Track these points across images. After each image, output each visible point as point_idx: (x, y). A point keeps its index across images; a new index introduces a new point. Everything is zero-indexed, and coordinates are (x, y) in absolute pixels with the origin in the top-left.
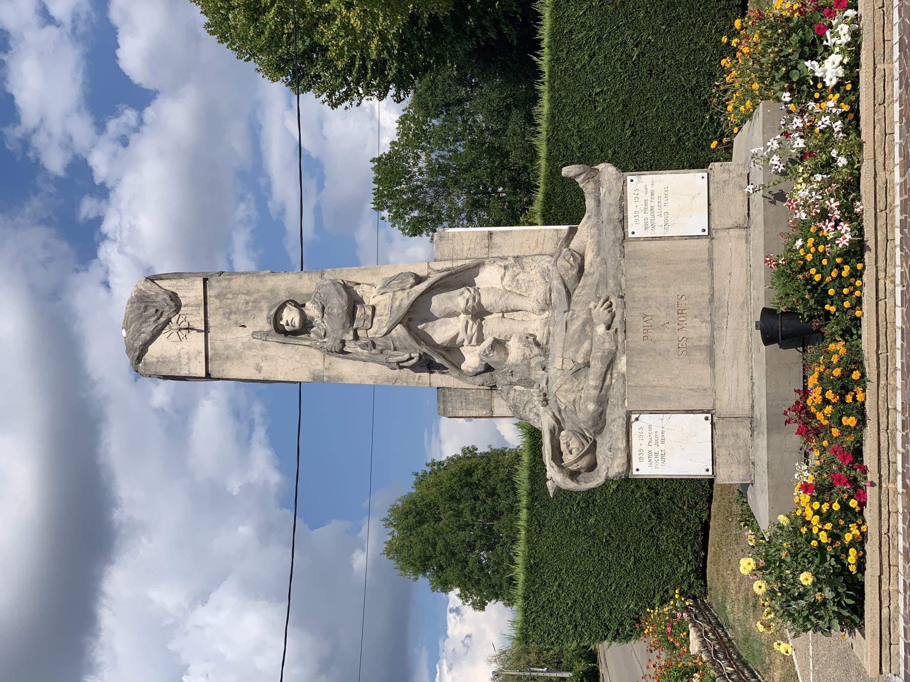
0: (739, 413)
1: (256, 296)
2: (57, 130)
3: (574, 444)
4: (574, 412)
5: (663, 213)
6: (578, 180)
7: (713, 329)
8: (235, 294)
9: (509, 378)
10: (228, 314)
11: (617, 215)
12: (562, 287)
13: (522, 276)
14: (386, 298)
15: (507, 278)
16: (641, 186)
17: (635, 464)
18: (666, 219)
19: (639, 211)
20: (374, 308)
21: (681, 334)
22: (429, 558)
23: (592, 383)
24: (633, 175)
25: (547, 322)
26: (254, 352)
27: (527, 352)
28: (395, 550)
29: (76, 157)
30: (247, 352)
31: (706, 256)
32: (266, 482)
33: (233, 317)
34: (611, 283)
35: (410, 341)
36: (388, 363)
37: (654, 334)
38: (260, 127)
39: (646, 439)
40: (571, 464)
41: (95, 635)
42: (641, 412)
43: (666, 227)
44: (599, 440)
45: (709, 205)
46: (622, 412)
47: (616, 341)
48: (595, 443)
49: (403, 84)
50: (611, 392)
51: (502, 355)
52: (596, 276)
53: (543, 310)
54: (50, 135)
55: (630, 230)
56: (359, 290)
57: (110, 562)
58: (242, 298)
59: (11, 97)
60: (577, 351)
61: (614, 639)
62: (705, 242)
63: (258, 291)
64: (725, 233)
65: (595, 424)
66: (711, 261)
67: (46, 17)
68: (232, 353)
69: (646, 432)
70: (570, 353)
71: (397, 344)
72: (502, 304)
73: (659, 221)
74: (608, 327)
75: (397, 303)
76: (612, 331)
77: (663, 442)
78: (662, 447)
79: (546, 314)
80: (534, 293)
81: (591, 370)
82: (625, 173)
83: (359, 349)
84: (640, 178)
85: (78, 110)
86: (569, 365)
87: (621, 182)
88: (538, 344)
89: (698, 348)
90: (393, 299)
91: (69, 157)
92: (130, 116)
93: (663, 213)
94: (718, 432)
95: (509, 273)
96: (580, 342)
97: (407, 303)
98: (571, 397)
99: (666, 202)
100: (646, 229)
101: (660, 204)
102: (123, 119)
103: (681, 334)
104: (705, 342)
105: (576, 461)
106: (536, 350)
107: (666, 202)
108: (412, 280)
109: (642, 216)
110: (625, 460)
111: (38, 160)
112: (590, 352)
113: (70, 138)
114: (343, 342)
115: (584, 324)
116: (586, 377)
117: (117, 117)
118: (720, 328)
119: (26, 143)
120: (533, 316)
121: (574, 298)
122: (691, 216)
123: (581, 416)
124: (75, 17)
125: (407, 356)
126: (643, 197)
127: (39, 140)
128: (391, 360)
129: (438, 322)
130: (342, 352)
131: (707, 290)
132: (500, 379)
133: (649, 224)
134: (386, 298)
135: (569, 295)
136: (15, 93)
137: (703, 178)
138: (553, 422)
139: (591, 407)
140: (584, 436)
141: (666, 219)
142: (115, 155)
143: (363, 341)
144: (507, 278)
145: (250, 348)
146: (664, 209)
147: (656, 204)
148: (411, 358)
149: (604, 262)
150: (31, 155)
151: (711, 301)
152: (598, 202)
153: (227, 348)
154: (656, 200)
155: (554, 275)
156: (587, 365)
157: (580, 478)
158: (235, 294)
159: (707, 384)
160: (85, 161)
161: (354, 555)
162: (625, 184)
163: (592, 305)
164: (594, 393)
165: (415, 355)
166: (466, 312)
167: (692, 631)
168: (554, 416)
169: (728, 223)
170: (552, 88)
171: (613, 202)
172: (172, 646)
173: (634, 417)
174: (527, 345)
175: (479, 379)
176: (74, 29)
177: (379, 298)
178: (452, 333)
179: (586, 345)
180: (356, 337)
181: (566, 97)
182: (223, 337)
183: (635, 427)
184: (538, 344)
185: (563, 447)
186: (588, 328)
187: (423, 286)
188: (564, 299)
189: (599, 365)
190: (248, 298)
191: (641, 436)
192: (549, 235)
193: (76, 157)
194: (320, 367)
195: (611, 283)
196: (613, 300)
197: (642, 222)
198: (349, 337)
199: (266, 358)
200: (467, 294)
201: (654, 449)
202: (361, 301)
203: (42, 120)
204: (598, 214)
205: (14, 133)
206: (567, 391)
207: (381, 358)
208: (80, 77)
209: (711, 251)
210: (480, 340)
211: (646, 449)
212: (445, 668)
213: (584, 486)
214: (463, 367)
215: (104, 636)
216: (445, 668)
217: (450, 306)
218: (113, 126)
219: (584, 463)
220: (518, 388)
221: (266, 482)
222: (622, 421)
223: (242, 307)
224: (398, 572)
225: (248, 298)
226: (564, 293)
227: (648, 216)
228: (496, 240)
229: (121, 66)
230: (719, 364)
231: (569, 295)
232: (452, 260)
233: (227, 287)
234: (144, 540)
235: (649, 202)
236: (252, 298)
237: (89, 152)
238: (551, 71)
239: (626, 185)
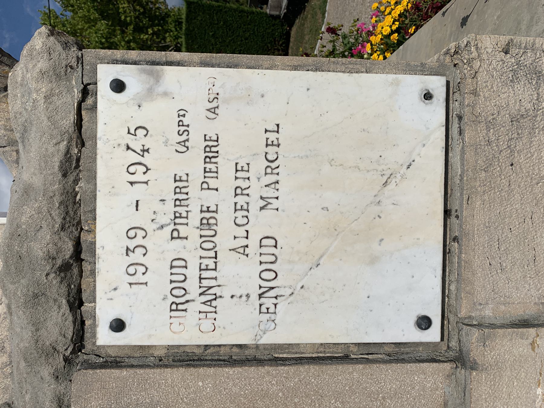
5: (254, 242)
19: (150, 227)
24: (125, 62)
43: (268, 303)
45: (447, 213)
82: (89, 54)
84: (157, 78)
87: (70, 90)
93: (254, 242)
99: (270, 193)
100: (175, 307)
101: (241, 200)
107: (270, 193)
122: (373, 260)
133: (193, 286)
137: (428, 96)
162: (89, 101)
171: (37, 181)
235: (194, 189)
239: (94, 107)
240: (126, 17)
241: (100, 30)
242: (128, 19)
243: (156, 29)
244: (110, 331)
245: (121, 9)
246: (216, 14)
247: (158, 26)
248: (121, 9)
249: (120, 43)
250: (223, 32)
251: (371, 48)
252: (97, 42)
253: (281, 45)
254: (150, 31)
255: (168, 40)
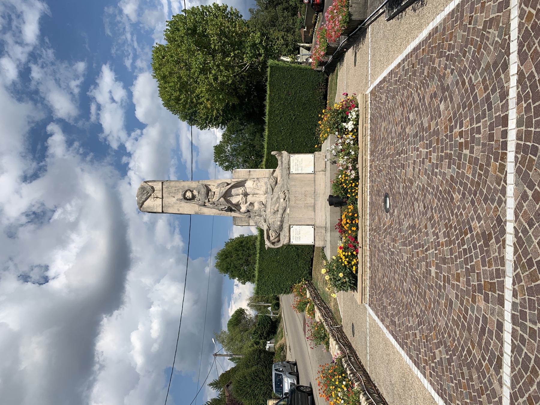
0: (322, 226)
1: (178, 188)
2: (116, 136)
3: (274, 234)
4: (274, 224)
6: (276, 156)
7: (315, 201)
8: (172, 187)
9: (255, 214)
10: (169, 193)
11: (287, 167)
12: (271, 187)
13: (259, 184)
14: (218, 190)
15: (255, 184)
16: (294, 158)
17: (291, 240)
18: (302, 168)
20: (214, 192)
21: (306, 202)
22: (229, 269)
23: (279, 216)
25: (266, 198)
26: (177, 205)
27: (260, 206)
28: (218, 266)
29: (121, 144)
30: (175, 205)
31: (313, 179)
32: (179, 245)
33: (171, 194)
34: (285, 186)
35: (225, 203)
36: (218, 209)
37: (298, 202)
38: (179, 136)
39: (295, 233)
40: (272, 240)
41: (124, 293)
42: (294, 225)
44: (281, 233)
46: (288, 225)
47: (286, 204)
48: (280, 234)
49: (223, 123)
50: (285, 219)
51: (253, 207)
52: (281, 184)
53: (265, 194)
54: (113, 137)
55: (291, 171)
56: (210, 187)
57: (129, 270)
58: (174, 189)
59: (101, 125)
60: (275, 206)
61: (284, 293)
62: (313, 175)
63: (179, 186)
64: (319, 173)
65: (280, 228)
66: (315, 181)
67: (113, 100)
68: (170, 205)
69: (295, 231)
70: (273, 207)
71: (221, 203)
72: (253, 192)
73: (300, 168)
74: (284, 200)
75: (221, 191)
76: (285, 201)
77: (300, 234)
78: (299, 235)
79: (266, 195)
80: (262, 189)
81: (279, 212)
83: (210, 205)
85: (122, 129)
86: (272, 211)
88: (263, 204)
89: (310, 206)
90: (220, 190)
91: (119, 144)
92: (138, 131)
94: (316, 231)
95: (255, 183)
96: (276, 204)
97: (224, 191)
98: (273, 220)
102: (136, 132)
103: (306, 202)
104: (312, 205)
105: (274, 239)
106: (263, 206)
108: (226, 184)
109: (295, 167)
110: (288, 239)
111: (109, 144)
112: (279, 207)
113: (120, 138)
114: (205, 202)
115: (277, 199)
116: (277, 214)
117: (135, 132)
118: (317, 201)
119: (105, 139)
120: (262, 196)
121: (274, 191)
123: (276, 226)
124: (122, 100)
125: (224, 207)
126: (295, 161)
127: (110, 138)
128: (219, 208)
129: (234, 197)
130: (204, 205)
131: (313, 189)
132: (252, 215)
134: (218, 190)
135: (273, 190)
136: (102, 123)
138: (267, 227)
139: (279, 223)
140: (276, 232)
141: (302, 168)
142: (133, 143)
143: (211, 202)
144: (255, 184)
145: (176, 204)
146: (301, 165)
147: (299, 164)
148: (225, 208)
149: (283, 180)
150: (107, 143)
151: (315, 192)
152: (282, 162)
153: (169, 203)
154: (299, 162)
155: (268, 184)
156: (278, 211)
157: (275, 244)
158: (172, 187)
159: (313, 217)
160: (124, 145)
161: (206, 268)
163: (279, 193)
164: (280, 219)
165: (227, 207)
166: (242, 194)
167: (307, 291)
168: (268, 226)
169: (320, 170)
170: (269, 128)
172: (149, 296)
173: (291, 226)
174: (260, 204)
175: (246, 214)
176: (122, 104)
177: (216, 189)
178: (238, 201)
179: (278, 205)
180: (209, 201)
181: (273, 130)
182: (168, 200)
183: (292, 229)
184: (263, 204)
185: (270, 235)
186: (278, 200)
187: (229, 186)
188: (271, 191)
189: (281, 211)
190: (176, 188)
191: (293, 232)
192: (267, 172)
193: (121, 144)
194: (198, 210)
195: (285, 186)
196: (286, 192)
197: (295, 169)
198: (207, 201)
199: (181, 207)
200: (242, 189)
201: (297, 236)
202: (210, 190)
203: (111, 132)
204: (282, 166)
205: (101, 136)
206: (271, 218)
207: (216, 207)
208: (123, 119)
209: (315, 178)
210: (246, 202)
211: (295, 236)
212: (233, 303)
213: (276, 247)
214: (241, 210)
215: (127, 293)
216: (233, 303)
217: (238, 192)
218: (133, 134)
219: (276, 240)
220: (257, 217)
221: (179, 245)
222: (288, 228)
223: (174, 191)
224: (219, 272)
225: (176, 188)
226: (271, 189)
227: (296, 167)
228: (251, 173)
229: (136, 116)
230: (316, 211)
231: (273, 190)
232: (238, 179)
233: (169, 185)
234: (140, 263)
236: (177, 189)
237: (125, 142)
238: (268, 122)
240: (215, 46)
241: (198, 59)
242: (217, 47)
243: (236, 52)
244: (113, 315)
245: (212, 41)
246: (286, 72)
247: (238, 50)
248: (212, 41)
249: (213, 67)
250: (290, 81)
251: (281, 231)
252: (196, 68)
253: (323, 86)
254: (232, 54)
255: (245, 59)
